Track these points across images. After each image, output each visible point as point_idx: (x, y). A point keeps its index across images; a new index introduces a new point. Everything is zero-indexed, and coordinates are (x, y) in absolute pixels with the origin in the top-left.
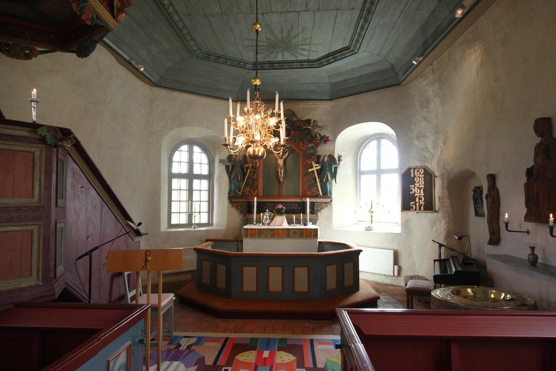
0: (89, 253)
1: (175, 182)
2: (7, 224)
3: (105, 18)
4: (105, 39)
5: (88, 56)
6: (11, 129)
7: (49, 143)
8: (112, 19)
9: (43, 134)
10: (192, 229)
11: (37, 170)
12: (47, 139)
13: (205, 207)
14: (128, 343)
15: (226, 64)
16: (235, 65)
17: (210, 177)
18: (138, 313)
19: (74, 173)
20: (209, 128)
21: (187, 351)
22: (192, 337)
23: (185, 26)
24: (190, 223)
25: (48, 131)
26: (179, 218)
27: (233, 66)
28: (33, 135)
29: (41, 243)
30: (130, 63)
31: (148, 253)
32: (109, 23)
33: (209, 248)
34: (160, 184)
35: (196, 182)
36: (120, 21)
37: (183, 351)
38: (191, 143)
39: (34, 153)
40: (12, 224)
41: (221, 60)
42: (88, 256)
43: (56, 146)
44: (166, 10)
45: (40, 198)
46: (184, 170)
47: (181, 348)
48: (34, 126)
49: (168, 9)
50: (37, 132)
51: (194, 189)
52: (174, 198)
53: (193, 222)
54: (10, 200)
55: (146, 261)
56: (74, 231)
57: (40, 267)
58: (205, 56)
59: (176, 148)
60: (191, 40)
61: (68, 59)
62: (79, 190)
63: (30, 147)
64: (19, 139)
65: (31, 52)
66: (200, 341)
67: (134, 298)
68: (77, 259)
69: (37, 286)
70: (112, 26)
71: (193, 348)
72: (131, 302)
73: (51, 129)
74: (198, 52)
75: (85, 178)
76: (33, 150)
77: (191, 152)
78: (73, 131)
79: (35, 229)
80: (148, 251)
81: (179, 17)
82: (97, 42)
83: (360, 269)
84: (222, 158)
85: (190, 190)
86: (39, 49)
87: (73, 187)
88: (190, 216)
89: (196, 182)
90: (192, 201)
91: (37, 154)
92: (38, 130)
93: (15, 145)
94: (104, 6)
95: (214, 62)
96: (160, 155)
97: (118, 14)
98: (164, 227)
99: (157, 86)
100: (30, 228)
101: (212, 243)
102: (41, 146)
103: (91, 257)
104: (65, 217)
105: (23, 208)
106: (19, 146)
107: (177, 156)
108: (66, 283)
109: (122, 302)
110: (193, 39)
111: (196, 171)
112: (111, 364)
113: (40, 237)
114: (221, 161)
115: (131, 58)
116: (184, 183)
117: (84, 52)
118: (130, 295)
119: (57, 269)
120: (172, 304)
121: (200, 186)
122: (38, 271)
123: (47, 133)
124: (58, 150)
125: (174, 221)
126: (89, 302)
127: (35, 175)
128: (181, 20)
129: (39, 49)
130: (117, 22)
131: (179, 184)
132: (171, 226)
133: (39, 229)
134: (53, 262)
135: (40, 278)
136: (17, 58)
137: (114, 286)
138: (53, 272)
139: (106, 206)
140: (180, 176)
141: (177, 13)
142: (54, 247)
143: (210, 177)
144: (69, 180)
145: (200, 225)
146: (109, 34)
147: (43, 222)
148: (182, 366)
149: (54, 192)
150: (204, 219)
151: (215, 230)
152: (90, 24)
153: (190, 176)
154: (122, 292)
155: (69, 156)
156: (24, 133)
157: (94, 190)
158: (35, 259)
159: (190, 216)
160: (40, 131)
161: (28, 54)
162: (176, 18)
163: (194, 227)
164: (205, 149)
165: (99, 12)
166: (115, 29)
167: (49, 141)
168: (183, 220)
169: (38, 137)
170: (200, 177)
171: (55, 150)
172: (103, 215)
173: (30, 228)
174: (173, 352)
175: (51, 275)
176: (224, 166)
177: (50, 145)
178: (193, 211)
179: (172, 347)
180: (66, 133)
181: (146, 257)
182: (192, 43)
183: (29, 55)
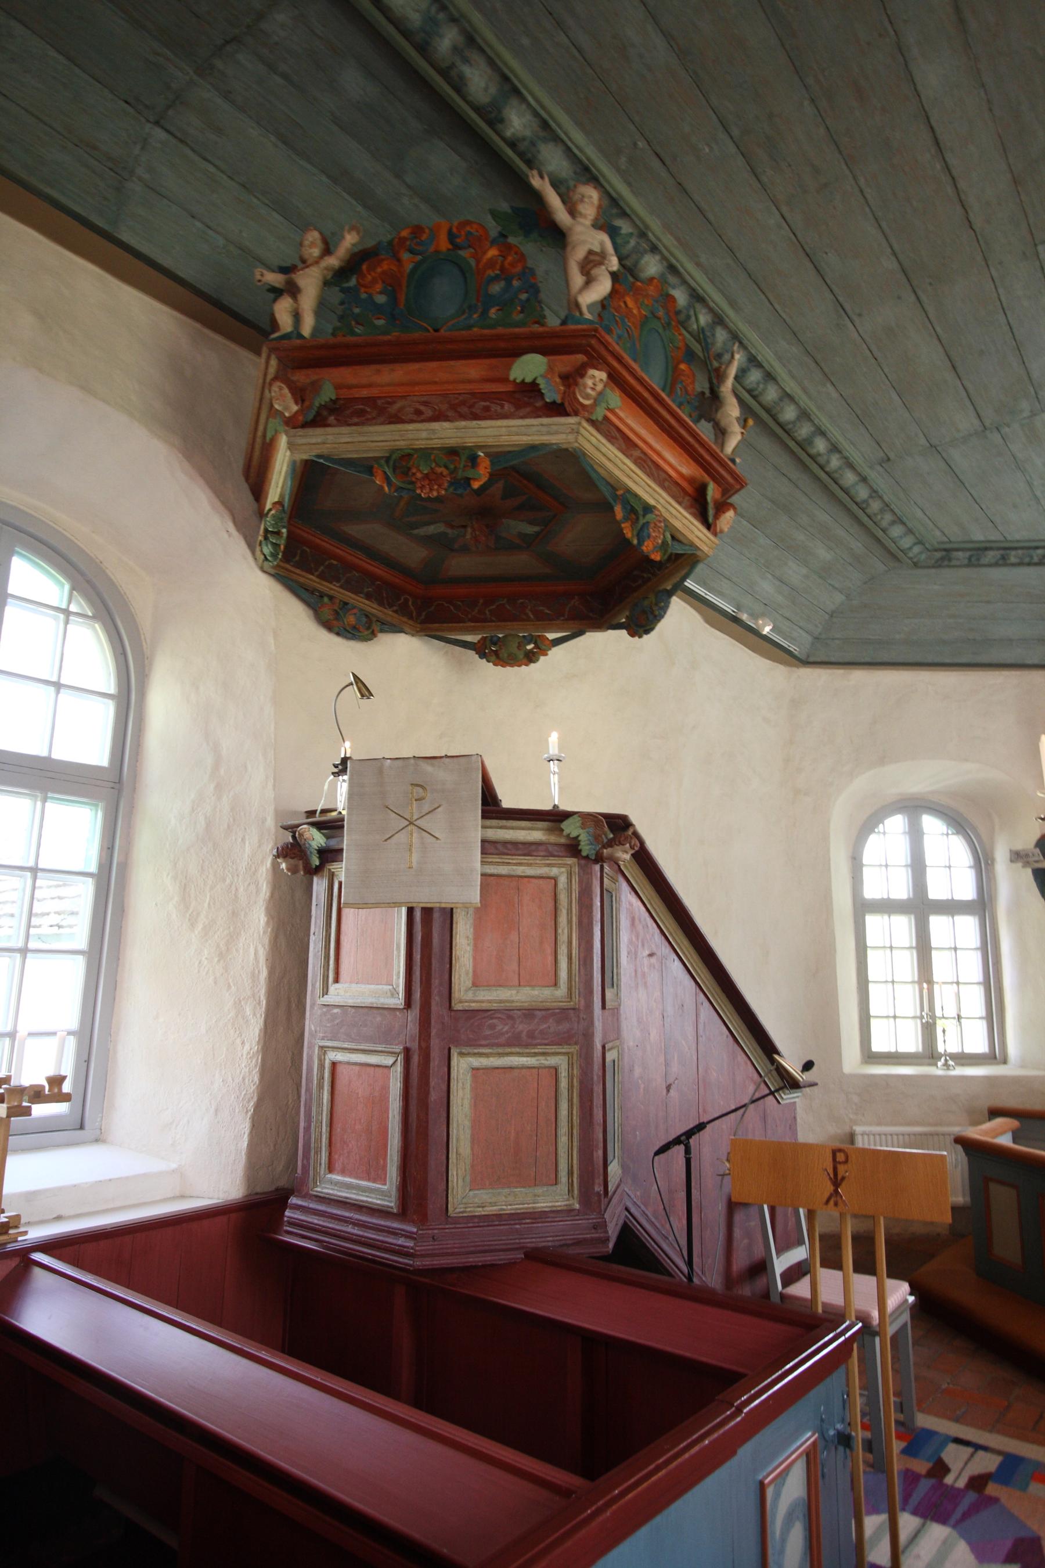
0: (684, 1139)
1: (874, 923)
2: (509, 1050)
3: (691, 537)
4: (689, 583)
5: (652, 629)
6: (512, 828)
7: (584, 854)
8: (705, 531)
9: (574, 834)
10: (938, 1071)
11: (563, 919)
12: (582, 843)
13: (974, 1001)
14: (808, 1438)
15: (1006, 565)
16: (1036, 559)
17: (982, 906)
18: (829, 1345)
19: (633, 920)
20: (966, 760)
21: (971, 1497)
22: (985, 1448)
23: (875, 493)
24: (930, 1054)
25: (583, 826)
26: (895, 1034)
27: (1029, 564)
28: (553, 839)
29: (576, 1100)
30: (735, 620)
31: (840, 1157)
32: (698, 543)
33: (1005, 1140)
34: (833, 932)
35: (937, 924)
36: (721, 531)
37: (955, 1495)
38: (914, 807)
39: (555, 879)
40: (518, 1050)
41: (991, 556)
42: (682, 1147)
43: (599, 859)
44: (822, 467)
45: (570, 989)
46: (901, 889)
47: (949, 1480)
48: (556, 817)
49: (828, 462)
50: (562, 830)
51: (933, 945)
52: (874, 972)
53: (941, 1049)
54: (514, 992)
55: (836, 1182)
56: (638, 1071)
57: (575, 1162)
58: (938, 555)
59: (869, 824)
60: (893, 523)
61: (605, 646)
62: (646, 961)
63: (549, 865)
64: (527, 849)
65: (537, 646)
66: (1011, 1468)
67: (793, 1274)
68: (657, 1153)
69: (570, 1211)
70: (705, 549)
71: (992, 1489)
72: (784, 1286)
73: (589, 819)
74: (916, 549)
75: (657, 931)
76: (554, 871)
77: (916, 835)
78: (633, 819)
79: (560, 1062)
80: (840, 1150)
81: (859, 474)
82: (670, 594)
83: (927, 863)
84: (1019, 846)
85: (923, 948)
86: (551, 636)
87: (633, 955)
88: (929, 1030)
89: (937, 924)
90: (930, 982)
91: (563, 880)
92: (564, 825)
93: (520, 864)
94: (685, 508)
95: (968, 566)
96: (828, 851)
97: (717, 516)
98: (851, 1061)
99: (806, 662)
100: (552, 1061)
101: (1014, 1123)
102: (570, 861)
103: (688, 1151)
104: (618, 1037)
105: (538, 1013)
106: (529, 865)
107: (874, 848)
108: (627, 1209)
109: (760, 1283)
110: (899, 520)
111: (936, 892)
112: (770, 1492)
113: (572, 1086)
114: (1017, 856)
115: (739, 608)
116: (902, 927)
117: (641, 624)
118: (781, 1264)
119: (609, 1169)
120: (906, 1317)
121: (957, 936)
122: (570, 1173)
123: (581, 831)
124: (602, 868)
125: (879, 1045)
126: (690, 1279)
127: (560, 931)
128: (864, 479)
129: (551, 636)
130: (715, 534)
131: (892, 932)
132: (871, 1057)
133: (571, 1065)
134: (600, 1152)
135: (576, 1192)
136: (512, 666)
137: (737, 1233)
138: (602, 1178)
139: (706, 1004)
140: (887, 907)
141: (851, 466)
142: (601, 1113)
143: (982, 906)
144: (625, 937)
145: (964, 1059)
146: (700, 568)
147: (577, 1047)
148: (962, 1550)
149: (596, 971)
150: (977, 1042)
151: (1016, 1080)
152: (658, 558)
153: (921, 907)
154: (758, 1252)
155: (621, 879)
156: (535, 834)
157: (677, 962)
158: (563, 1140)
159: (929, 1030)
160: (571, 828)
161: (531, 651)
162: (849, 478)
163: (946, 1064)
164: (958, 823)
165: (677, 524)
166: (711, 553)
167: (586, 849)
168: (910, 1042)
169: (563, 841)
170: (951, 908)
171: (597, 867)
172: (701, 1027)
173: (552, 1061)
174: (924, 1486)
175: (598, 1188)
176: (1029, 871)
177: (587, 857)
178: (938, 1013)
179: (921, 1466)
180: (618, 826)
181: (835, 1169)
182: (896, 531)
183: (534, 653)
